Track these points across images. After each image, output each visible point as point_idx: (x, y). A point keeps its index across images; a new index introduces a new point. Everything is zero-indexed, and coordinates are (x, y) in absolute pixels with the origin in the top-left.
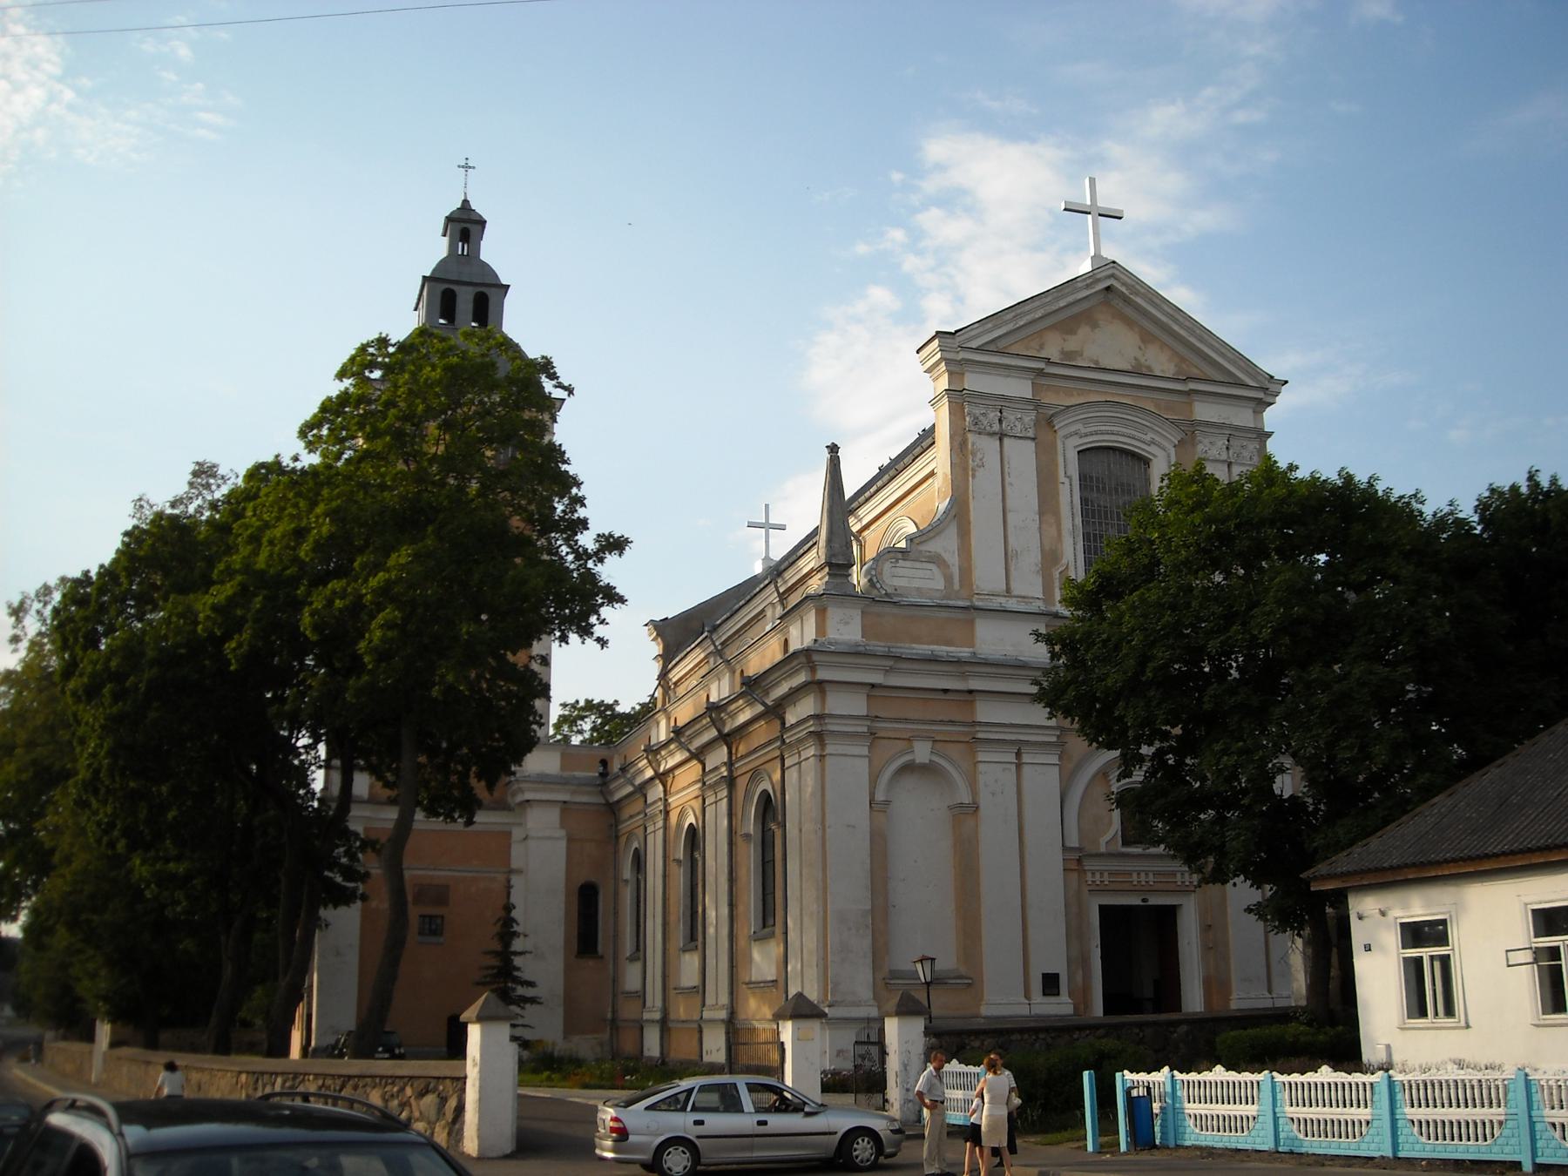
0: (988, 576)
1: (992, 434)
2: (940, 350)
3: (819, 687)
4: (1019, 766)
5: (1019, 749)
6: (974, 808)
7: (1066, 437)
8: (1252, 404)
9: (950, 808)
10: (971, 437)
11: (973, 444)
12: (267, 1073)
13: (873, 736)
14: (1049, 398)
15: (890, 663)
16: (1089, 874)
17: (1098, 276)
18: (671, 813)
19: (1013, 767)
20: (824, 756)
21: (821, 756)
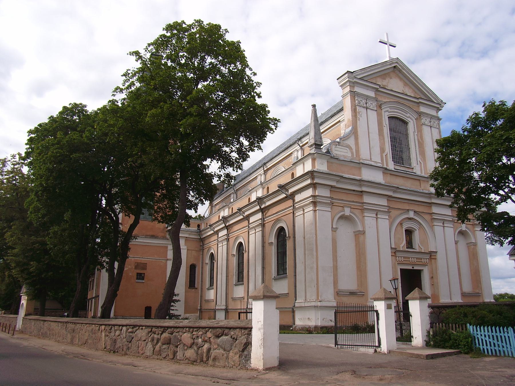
0: (364, 155)
1: (364, 107)
2: (348, 78)
3: (314, 186)
4: (377, 218)
5: (377, 212)
6: (363, 233)
7: (385, 112)
8: (436, 109)
9: (354, 232)
10: (358, 108)
11: (358, 110)
12: (117, 325)
13: (332, 204)
14: (379, 99)
15: (338, 178)
16: (398, 257)
17: (393, 62)
18: (230, 239)
19: (375, 219)
20: (316, 210)
21: (315, 210)
